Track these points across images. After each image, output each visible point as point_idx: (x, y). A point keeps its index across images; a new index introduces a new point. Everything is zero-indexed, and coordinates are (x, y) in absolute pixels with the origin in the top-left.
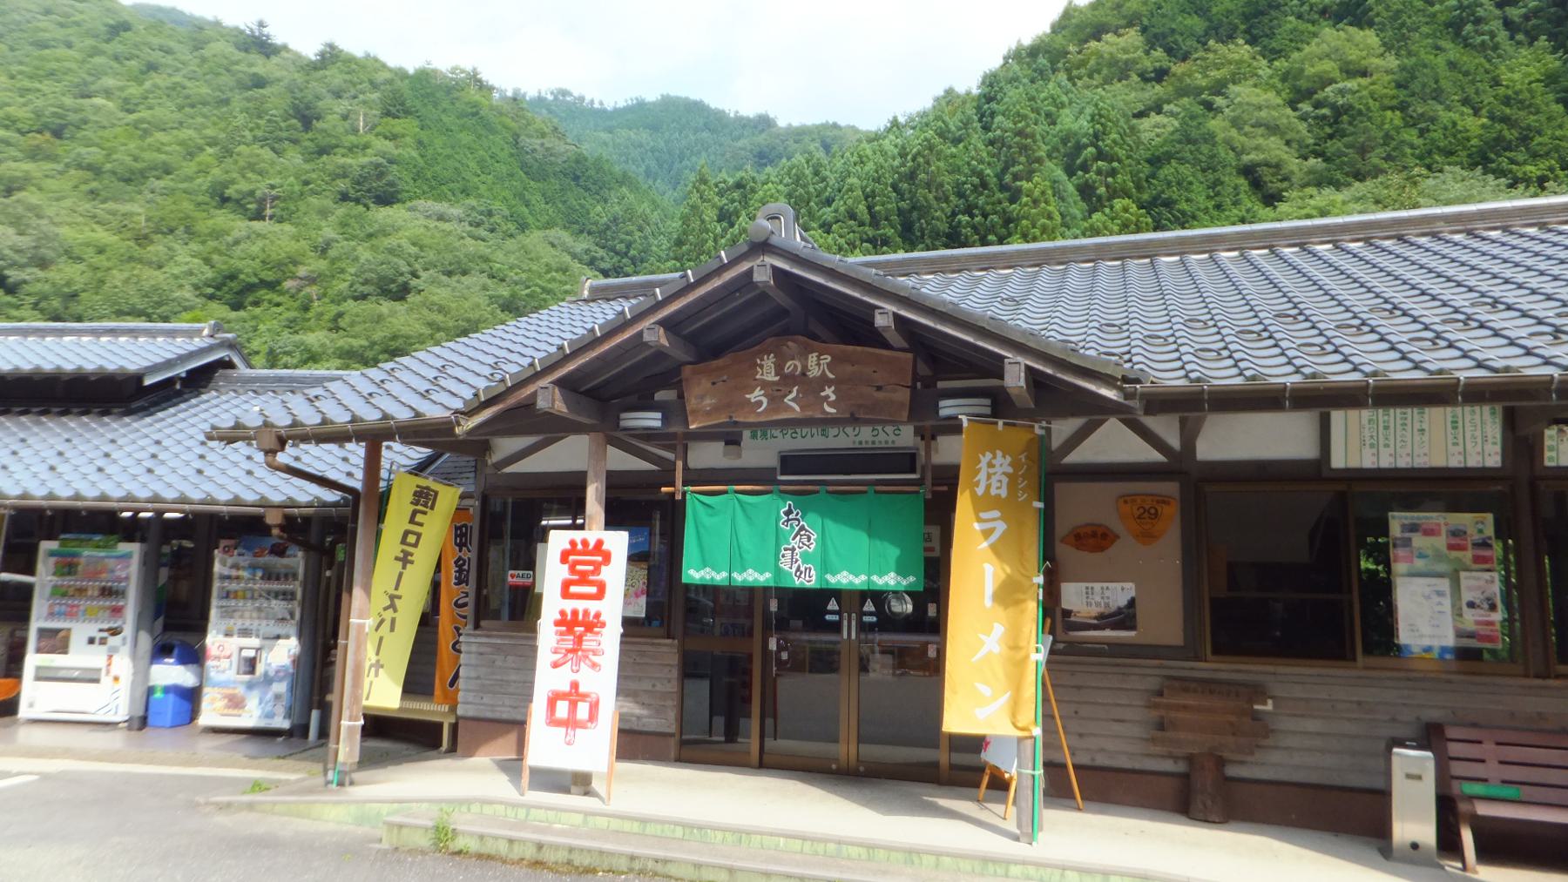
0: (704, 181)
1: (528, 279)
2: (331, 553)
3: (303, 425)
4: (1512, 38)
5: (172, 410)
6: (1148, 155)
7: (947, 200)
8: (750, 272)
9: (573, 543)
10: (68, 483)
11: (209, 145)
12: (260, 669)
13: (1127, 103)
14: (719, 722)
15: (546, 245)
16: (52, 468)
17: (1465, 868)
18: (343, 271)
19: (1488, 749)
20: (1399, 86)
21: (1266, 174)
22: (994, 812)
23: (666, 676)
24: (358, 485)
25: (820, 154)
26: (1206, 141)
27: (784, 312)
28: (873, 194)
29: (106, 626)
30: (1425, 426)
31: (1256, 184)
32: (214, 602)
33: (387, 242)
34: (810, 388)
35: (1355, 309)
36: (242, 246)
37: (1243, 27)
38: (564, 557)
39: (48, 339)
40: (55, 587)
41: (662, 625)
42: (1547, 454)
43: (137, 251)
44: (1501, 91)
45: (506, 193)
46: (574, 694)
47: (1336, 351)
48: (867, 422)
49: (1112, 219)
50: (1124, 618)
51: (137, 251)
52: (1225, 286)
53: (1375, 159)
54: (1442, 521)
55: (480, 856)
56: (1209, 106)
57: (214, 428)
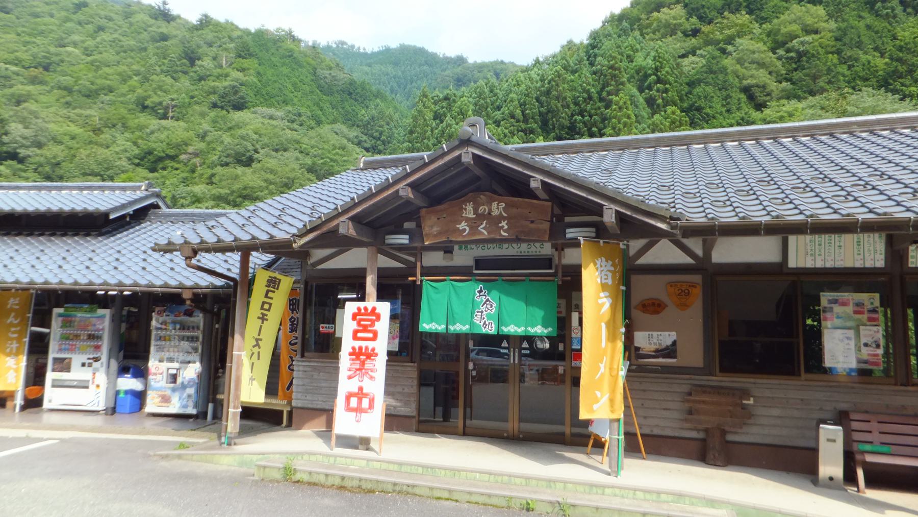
0: (425, 96)
1: (323, 154)
2: (218, 315)
3: (207, 243)
4: (905, 11)
5: (125, 233)
6: (687, 80)
7: (568, 107)
8: (460, 156)
9: (359, 309)
10: (70, 275)
11: (136, 75)
12: (179, 380)
13: (675, 49)
14: (440, 410)
15: (333, 134)
16: (60, 267)
17: (858, 491)
18: (214, 149)
19: (874, 426)
20: (837, 39)
21: (757, 92)
22: (595, 459)
23: (410, 383)
24: (237, 277)
25: (494, 80)
26: (722, 72)
27: (478, 178)
28: (524, 104)
29: (91, 356)
30: (842, 244)
31: (751, 98)
32: (153, 343)
33: (240, 132)
34: (494, 221)
35: (803, 178)
36: (156, 135)
37: (745, 4)
38: (354, 317)
39: (53, 192)
40: (62, 334)
41: (408, 355)
42: (910, 260)
43: (95, 138)
44: (898, 42)
45: (309, 103)
46: (361, 394)
47: (791, 202)
48: (524, 241)
49: (666, 119)
50: (670, 351)
51: (95, 138)
52: (729, 163)
53: (821, 83)
54: (850, 298)
55: (309, 484)
56: (724, 51)
57: (156, 244)
